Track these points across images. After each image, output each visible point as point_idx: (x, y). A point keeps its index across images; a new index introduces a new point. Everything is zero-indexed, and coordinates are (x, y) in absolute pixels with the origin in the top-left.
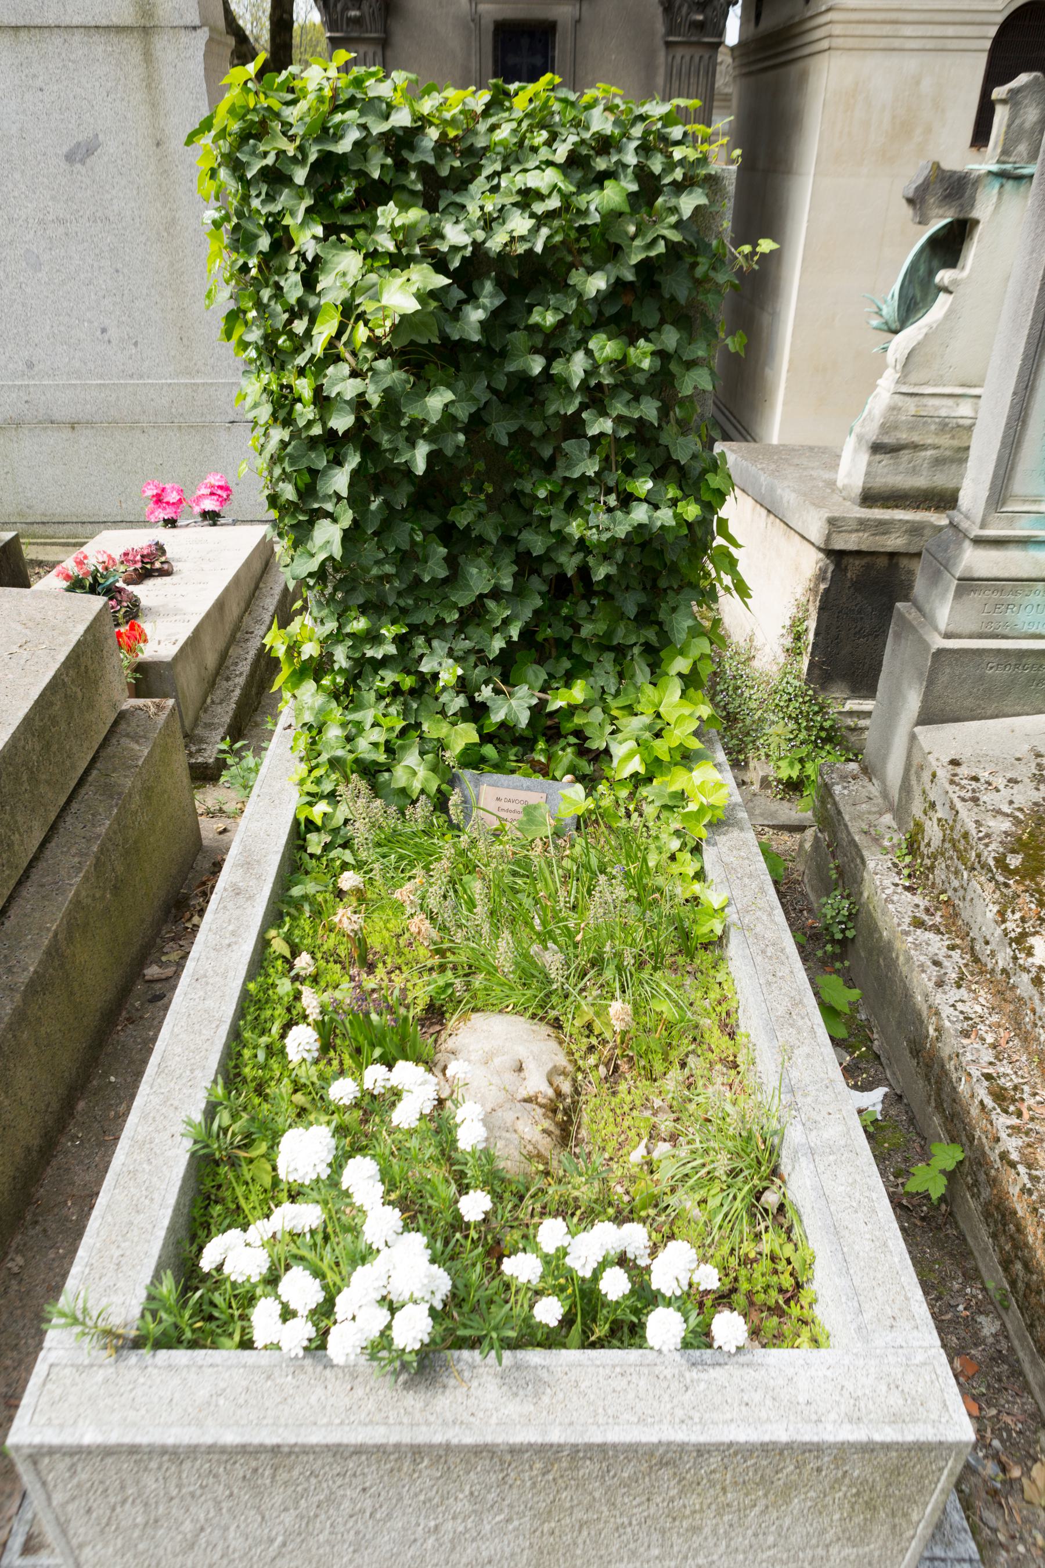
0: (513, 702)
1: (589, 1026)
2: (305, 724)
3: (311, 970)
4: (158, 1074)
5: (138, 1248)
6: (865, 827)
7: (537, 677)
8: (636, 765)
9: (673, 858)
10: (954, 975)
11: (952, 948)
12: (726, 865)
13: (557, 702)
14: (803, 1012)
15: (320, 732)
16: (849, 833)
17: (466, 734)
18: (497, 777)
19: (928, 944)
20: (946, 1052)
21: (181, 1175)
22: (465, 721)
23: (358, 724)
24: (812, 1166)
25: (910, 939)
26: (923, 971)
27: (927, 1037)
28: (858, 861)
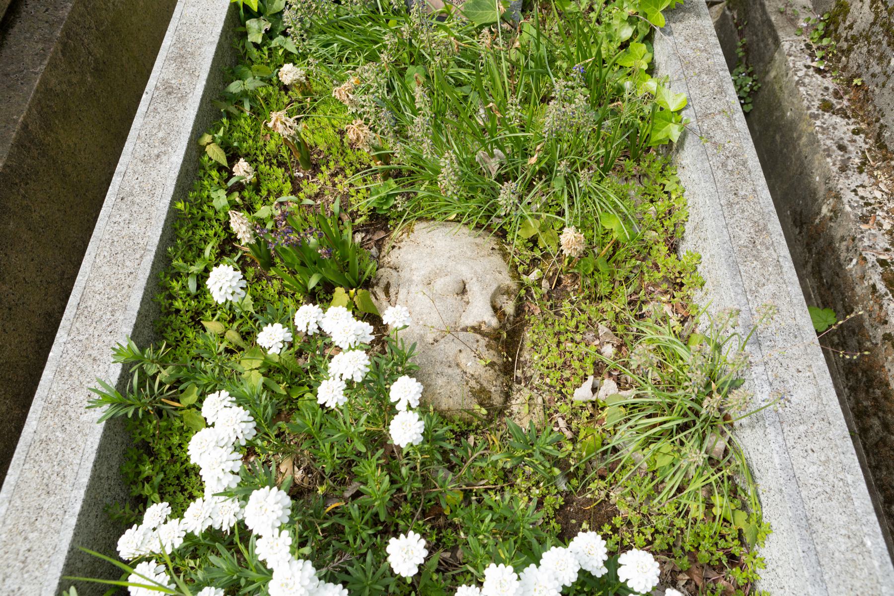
1: (534, 241)
3: (250, 178)
4: (76, 317)
5: (47, 541)
6: (782, 7)
9: (625, 45)
10: (857, 161)
11: (856, 132)
12: (681, 59)
14: (768, 241)
16: (764, 12)
19: (835, 128)
20: (839, 233)
21: (96, 446)
24: (780, 438)
25: (818, 123)
26: (829, 156)
27: (819, 213)
28: (770, 41)
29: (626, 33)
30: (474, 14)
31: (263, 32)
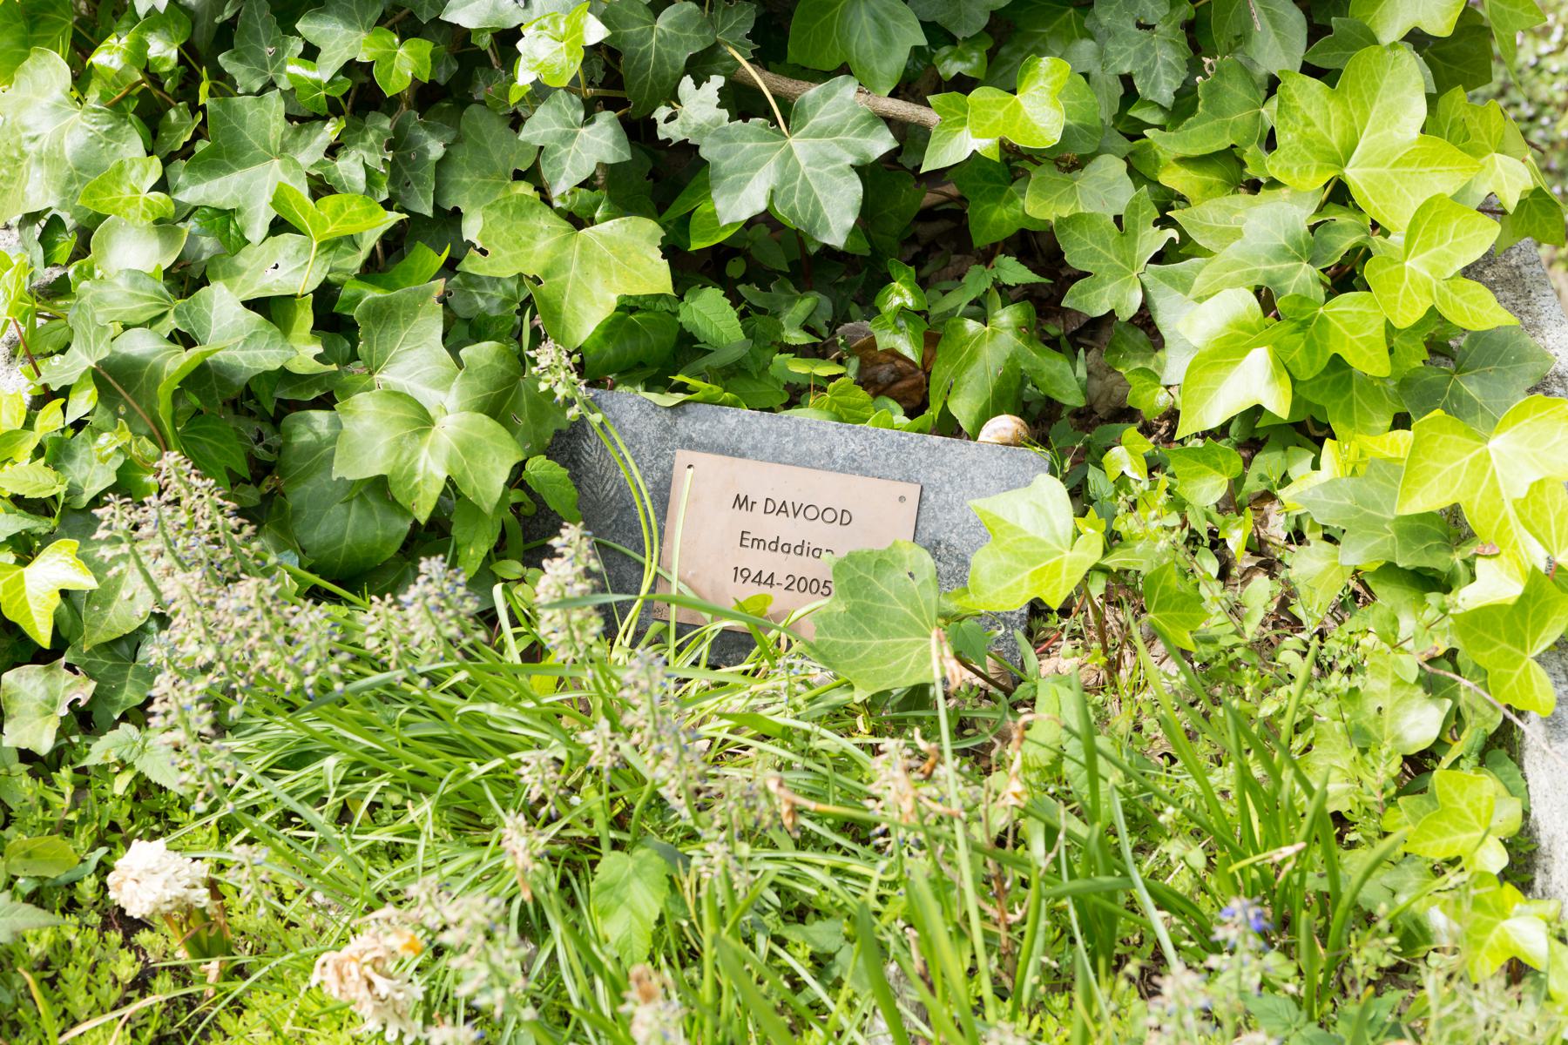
0: (799, 144)
2: (30, 218)
7: (885, 37)
8: (1258, 383)
9: (1419, 764)
13: (962, 137)
15: (82, 250)
17: (621, 263)
18: (737, 420)
22: (624, 206)
23: (224, 218)
29: (1421, 723)
30: (851, 652)
31: (63, 711)
